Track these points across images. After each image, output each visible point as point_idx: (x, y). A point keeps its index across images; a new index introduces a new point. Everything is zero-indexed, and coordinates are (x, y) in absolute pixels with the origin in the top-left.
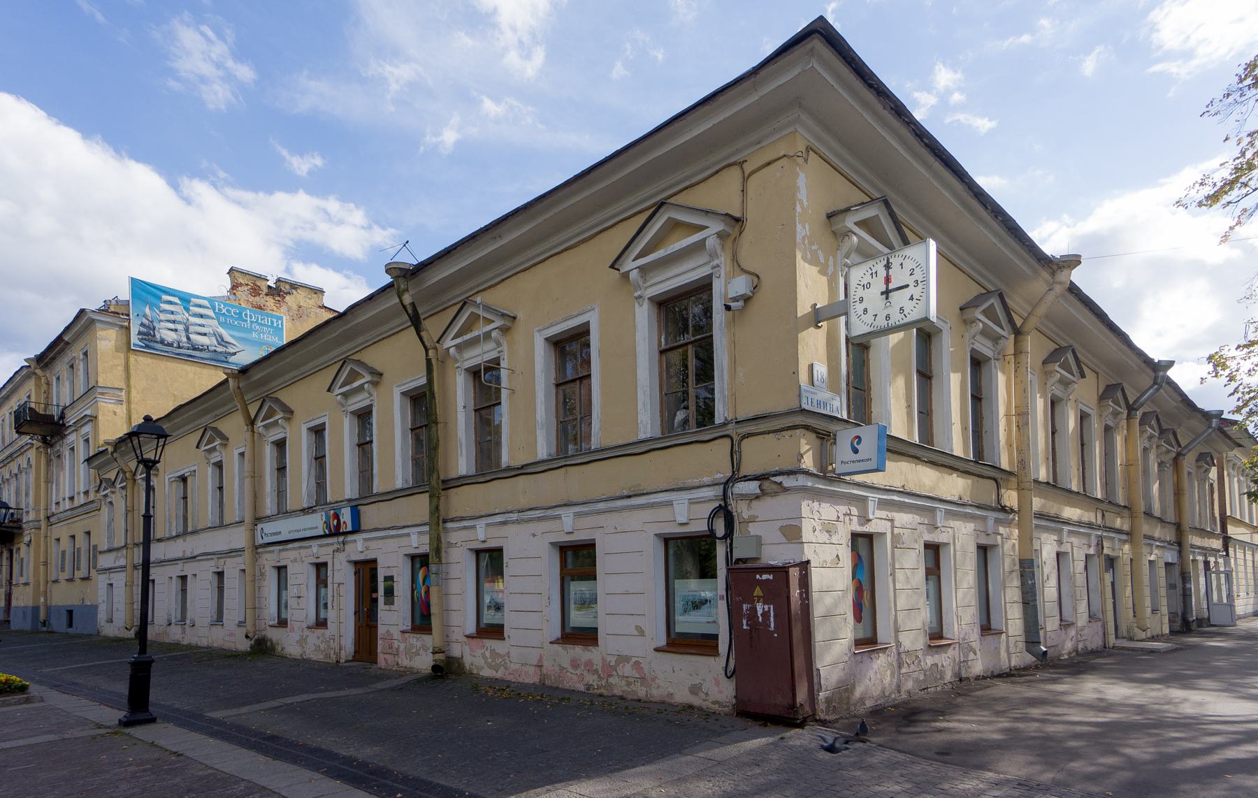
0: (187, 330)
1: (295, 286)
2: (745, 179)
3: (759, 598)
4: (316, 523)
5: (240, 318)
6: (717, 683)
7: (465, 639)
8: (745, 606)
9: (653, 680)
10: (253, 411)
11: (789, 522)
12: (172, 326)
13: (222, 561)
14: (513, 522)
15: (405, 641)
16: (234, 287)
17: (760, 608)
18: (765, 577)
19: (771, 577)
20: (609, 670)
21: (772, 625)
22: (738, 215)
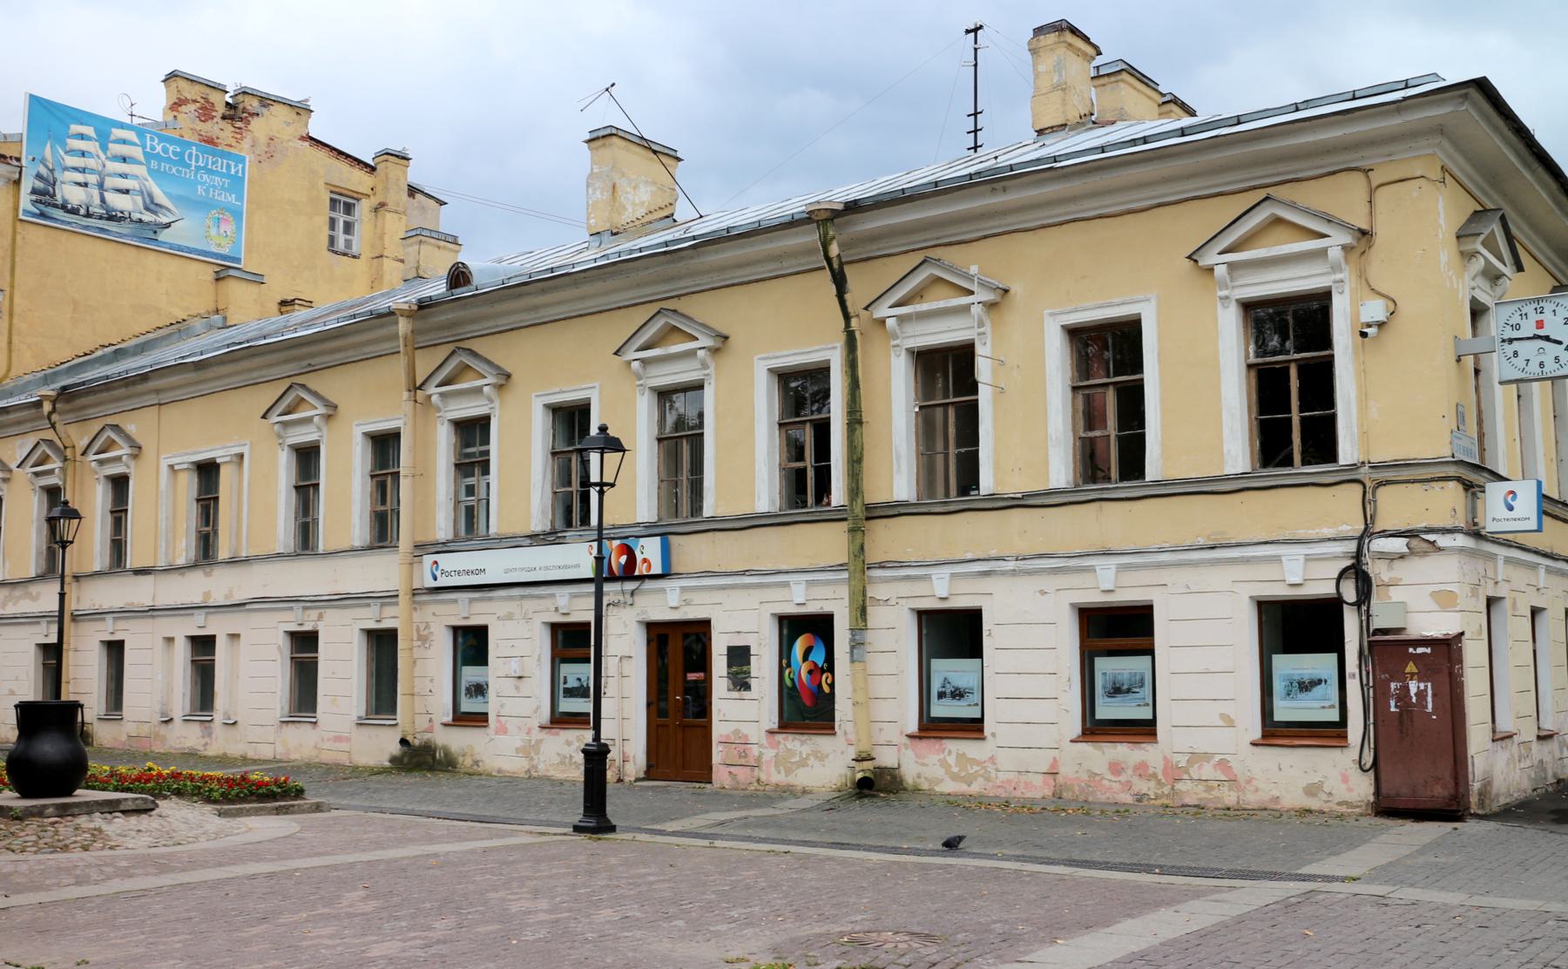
0: (101, 186)
1: (266, 101)
2: (1372, 192)
3: (1412, 674)
4: (577, 557)
5: (181, 162)
6: (1345, 779)
7: (907, 741)
8: (1393, 685)
9: (1249, 781)
10: (423, 367)
11: (1443, 587)
12: (80, 177)
13: (314, 614)
14: (1004, 573)
15: (775, 745)
16: (176, 105)
17: (1413, 687)
18: (1420, 650)
19: (1428, 650)
20: (1174, 774)
21: (1430, 706)
22: (1365, 227)
